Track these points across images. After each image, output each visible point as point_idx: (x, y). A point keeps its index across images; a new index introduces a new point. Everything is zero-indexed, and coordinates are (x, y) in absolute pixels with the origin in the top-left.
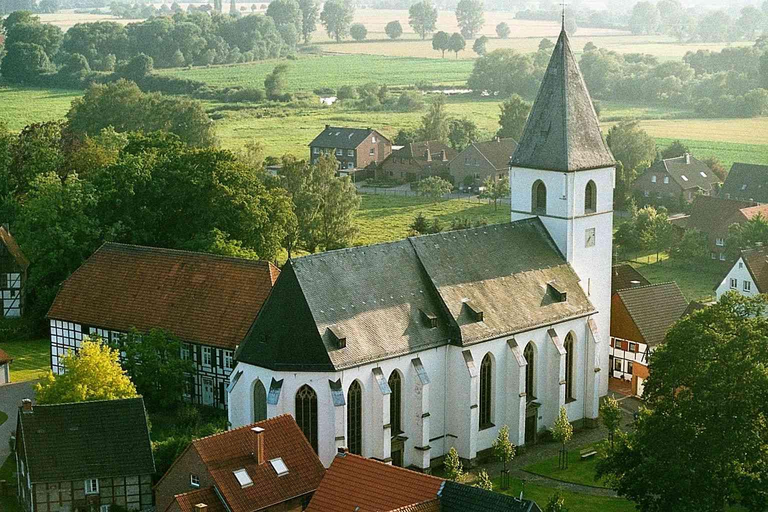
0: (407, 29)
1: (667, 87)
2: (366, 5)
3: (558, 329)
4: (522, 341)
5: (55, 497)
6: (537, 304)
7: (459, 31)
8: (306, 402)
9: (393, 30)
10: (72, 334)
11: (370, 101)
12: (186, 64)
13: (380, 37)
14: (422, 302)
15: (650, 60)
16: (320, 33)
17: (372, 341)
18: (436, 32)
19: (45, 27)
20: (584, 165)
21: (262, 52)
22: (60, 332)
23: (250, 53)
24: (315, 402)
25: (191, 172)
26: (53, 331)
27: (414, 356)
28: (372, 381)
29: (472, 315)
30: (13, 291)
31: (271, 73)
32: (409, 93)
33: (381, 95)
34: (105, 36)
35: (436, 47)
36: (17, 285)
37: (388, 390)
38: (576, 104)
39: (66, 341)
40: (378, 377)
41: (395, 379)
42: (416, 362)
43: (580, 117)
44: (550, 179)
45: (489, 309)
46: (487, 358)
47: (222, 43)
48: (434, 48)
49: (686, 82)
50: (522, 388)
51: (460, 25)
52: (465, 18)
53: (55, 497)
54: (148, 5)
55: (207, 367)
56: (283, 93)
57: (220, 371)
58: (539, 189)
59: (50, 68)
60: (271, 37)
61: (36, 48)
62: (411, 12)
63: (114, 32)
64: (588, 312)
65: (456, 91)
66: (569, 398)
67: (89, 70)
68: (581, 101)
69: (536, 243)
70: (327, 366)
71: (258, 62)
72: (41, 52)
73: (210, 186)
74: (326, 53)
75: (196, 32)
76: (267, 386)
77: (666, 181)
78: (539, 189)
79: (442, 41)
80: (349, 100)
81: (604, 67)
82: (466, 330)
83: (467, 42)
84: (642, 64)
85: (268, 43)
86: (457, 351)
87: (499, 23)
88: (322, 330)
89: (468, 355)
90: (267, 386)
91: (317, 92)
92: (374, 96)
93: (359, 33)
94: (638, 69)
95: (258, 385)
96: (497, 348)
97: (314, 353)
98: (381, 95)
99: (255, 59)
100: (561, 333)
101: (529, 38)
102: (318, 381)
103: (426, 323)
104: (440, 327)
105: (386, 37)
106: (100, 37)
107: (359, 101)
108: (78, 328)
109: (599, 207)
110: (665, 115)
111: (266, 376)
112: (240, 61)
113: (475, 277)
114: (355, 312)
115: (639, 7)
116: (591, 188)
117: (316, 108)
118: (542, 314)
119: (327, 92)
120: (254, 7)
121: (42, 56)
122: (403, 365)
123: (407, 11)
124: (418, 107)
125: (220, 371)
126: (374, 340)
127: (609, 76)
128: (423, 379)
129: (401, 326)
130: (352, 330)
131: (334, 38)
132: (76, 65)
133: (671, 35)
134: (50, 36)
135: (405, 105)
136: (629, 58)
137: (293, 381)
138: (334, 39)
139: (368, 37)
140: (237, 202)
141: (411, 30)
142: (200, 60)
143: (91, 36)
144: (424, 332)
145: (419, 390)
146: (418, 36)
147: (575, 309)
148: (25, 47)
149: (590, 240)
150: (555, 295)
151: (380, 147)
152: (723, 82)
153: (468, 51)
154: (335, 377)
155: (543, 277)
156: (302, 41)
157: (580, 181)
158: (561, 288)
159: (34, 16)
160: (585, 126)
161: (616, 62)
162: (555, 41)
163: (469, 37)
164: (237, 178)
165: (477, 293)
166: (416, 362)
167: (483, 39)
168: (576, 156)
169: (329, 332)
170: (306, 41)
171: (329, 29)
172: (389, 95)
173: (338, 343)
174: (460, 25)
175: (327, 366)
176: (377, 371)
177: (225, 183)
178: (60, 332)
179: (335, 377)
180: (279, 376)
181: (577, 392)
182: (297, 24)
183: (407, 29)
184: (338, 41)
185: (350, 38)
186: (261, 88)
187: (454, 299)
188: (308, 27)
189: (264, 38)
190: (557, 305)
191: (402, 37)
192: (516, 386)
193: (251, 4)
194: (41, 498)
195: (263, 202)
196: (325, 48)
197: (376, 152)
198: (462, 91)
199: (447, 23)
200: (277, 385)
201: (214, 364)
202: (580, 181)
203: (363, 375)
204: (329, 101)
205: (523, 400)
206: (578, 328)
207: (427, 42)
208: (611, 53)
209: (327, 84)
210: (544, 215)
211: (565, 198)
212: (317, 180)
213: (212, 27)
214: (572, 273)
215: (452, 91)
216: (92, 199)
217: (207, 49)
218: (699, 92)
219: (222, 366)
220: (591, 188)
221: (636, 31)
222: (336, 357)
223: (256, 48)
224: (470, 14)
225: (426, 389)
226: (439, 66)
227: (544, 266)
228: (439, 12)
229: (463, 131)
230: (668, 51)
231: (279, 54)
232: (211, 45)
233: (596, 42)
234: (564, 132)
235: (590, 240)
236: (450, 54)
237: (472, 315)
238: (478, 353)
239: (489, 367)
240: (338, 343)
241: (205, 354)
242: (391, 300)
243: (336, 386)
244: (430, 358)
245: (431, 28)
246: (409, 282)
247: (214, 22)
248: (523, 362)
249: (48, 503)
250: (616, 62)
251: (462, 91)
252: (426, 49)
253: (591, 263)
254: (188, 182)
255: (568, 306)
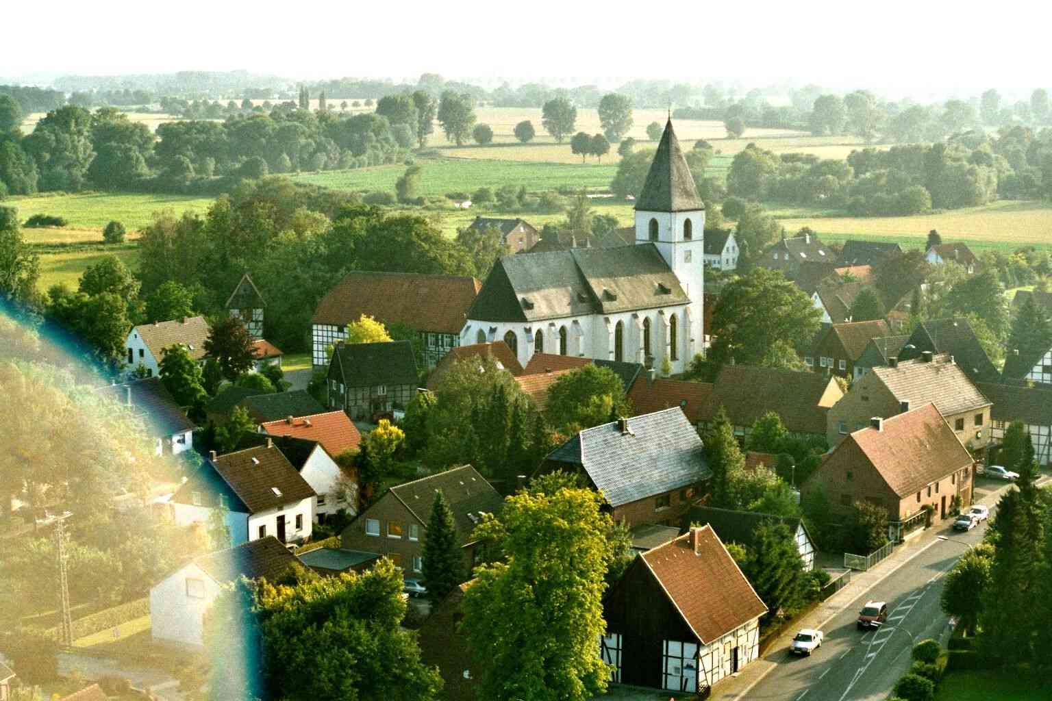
0: (541, 132)
1: (823, 187)
2: (485, 102)
3: (665, 310)
4: (642, 316)
5: (360, 396)
6: (652, 294)
7: (602, 132)
8: (511, 338)
9: (524, 132)
10: (330, 334)
11: (509, 203)
12: (293, 170)
13: (508, 141)
14: (579, 288)
15: (810, 159)
16: (437, 135)
17: (549, 305)
18: (575, 134)
19: (135, 126)
20: (684, 208)
21: (376, 157)
22: (320, 333)
23: (364, 158)
24: (515, 341)
25: (396, 232)
26: (315, 333)
27: (574, 319)
28: (549, 330)
29: (610, 297)
30: (257, 322)
31: (402, 175)
32: (550, 197)
33: (520, 197)
34: (202, 137)
35: (576, 150)
36: (261, 318)
37: (559, 336)
38: (678, 169)
39: (325, 339)
40: (553, 328)
41: (563, 330)
42: (575, 322)
43: (680, 177)
44: (661, 217)
45: (621, 295)
46: (619, 324)
47: (331, 145)
48: (574, 152)
49: (844, 182)
50: (642, 344)
51: (603, 126)
52: (610, 116)
53: (360, 396)
54: (211, 102)
55: (432, 348)
56: (415, 197)
57: (441, 349)
58: (654, 225)
59: (145, 171)
60: (386, 140)
61: (130, 149)
62: (545, 110)
63: (212, 132)
64: (685, 302)
65: (599, 196)
66: (674, 358)
67: (193, 174)
68: (681, 167)
69: (651, 258)
70: (523, 319)
71: (372, 168)
72: (135, 153)
73: (411, 243)
74: (449, 158)
75: (303, 133)
76: (486, 331)
77: (787, 257)
78: (654, 225)
79: (582, 144)
80: (487, 203)
81: (758, 168)
82: (607, 305)
83: (611, 145)
84: (799, 164)
85: (382, 147)
86: (601, 318)
87: (650, 123)
88: (520, 297)
89: (607, 320)
90: (486, 331)
91: (450, 197)
92: (514, 197)
93: (484, 136)
94: (793, 170)
95: (481, 333)
96: (626, 318)
97: (516, 311)
98: (520, 197)
99: (369, 164)
100: (668, 313)
101: (686, 141)
102: (518, 328)
103: (581, 300)
104: (589, 303)
105: (515, 140)
106: (197, 138)
107: (497, 204)
108: (335, 328)
109: (694, 237)
110: (815, 213)
111: (485, 326)
112: (352, 167)
113: (611, 275)
114: (539, 289)
115: (953, 105)
116: (688, 224)
117: (454, 210)
118: (655, 300)
119: (460, 197)
120: (344, 105)
121: (138, 159)
122: (568, 323)
123: (540, 110)
124: (559, 209)
125: (441, 349)
126: (551, 307)
127: (764, 177)
128: (579, 333)
129: (566, 300)
130: (535, 297)
131: (454, 141)
132: (179, 168)
133: (857, 135)
134: (141, 136)
135: (546, 206)
136: (786, 158)
137: (503, 329)
138: (454, 143)
139: (495, 140)
140: (432, 255)
141: (546, 133)
142: (308, 165)
143: (187, 136)
144: (580, 305)
145: (577, 339)
146: (553, 140)
147: (676, 299)
148: (119, 148)
149: (688, 257)
150: (663, 290)
151: (529, 236)
152: (883, 181)
153: (613, 156)
154: (528, 326)
155: (655, 280)
156: (417, 145)
157: (679, 220)
158: (668, 286)
159: (120, 113)
160: (684, 183)
161: (770, 162)
162: (663, 128)
163: (614, 140)
164: (431, 237)
165: (613, 285)
166: (575, 322)
167: (630, 141)
168: (678, 201)
169: (524, 299)
170: (422, 145)
171: (448, 131)
172: (527, 198)
173: (530, 306)
174: (603, 126)
175: (523, 319)
176: (552, 325)
177: (423, 240)
178: (320, 333)
179: (528, 326)
180: (494, 325)
181: (679, 354)
182: (411, 124)
183: (541, 132)
184: (459, 146)
185: (473, 141)
186: (393, 192)
187: (599, 286)
188: (425, 128)
189: (377, 141)
190: (665, 297)
191: (535, 140)
192: (638, 341)
193: (341, 101)
194: (352, 397)
195: (450, 256)
196: (447, 153)
197: (525, 240)
198: (605, 196)
199: (589, 123)
200: (493, 331)
201: (436, 344)
202: (679, 220)
203: (544, 326)
204: (467, 204)
205: (643, 351)
206: (679, 311)
207: (562, 147)
208: (767, 153)
209: (459, 189)
210: (657, 241)
211: (670, 229)
212: (485, 248)
213: (318, 127)
214: (675, 278)
215: (595, 196)
216: (322, 249)
217: (315, 152)
218: (855, 191)
219: (442, 346)
220: (688, 224)
221: (817, 133)
222: (528, 314)
223: (369, 152)
224: (615, 112)
225: (581, 338)
226: (581, 172)
227: (658, 272)
228: (578, 111)
229: (607, 226)
230: (834, 149)
231: (395, 158)
232: (320, 148)
233: (758, 144)
234: (669, 187)
235: (688, 257)
236: (591, 159)
237: (610, 297)
238: (614, 320)
239: (621, 331)
240: (530, 306)
241: (431, 339)
242: (558, 282)
243: (528, 331)
244: (583, 321)
245: (569, 130)
246: (569, 273)
247: (320, 122)
248: (642, 327)
249: (356, 400)
250: (770, 162)
251: (605, 196)
252: (564, 153)
253: (689, 273)
254: (393, 240)
255: (672, 297)
